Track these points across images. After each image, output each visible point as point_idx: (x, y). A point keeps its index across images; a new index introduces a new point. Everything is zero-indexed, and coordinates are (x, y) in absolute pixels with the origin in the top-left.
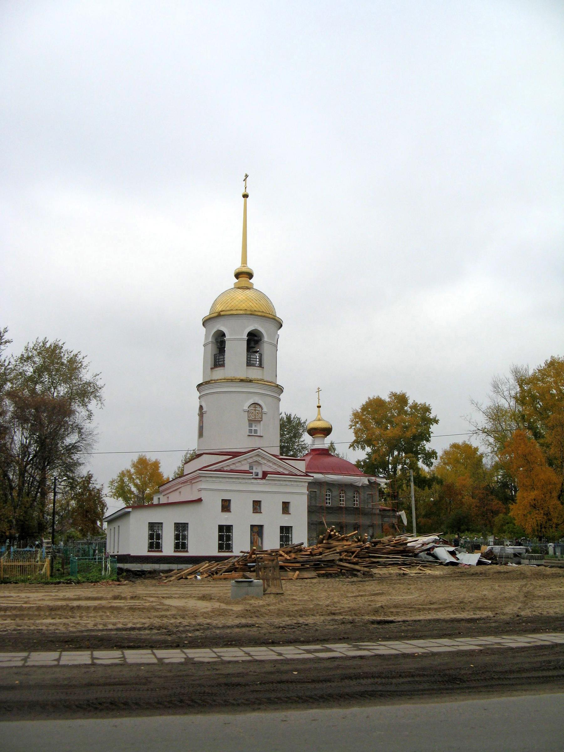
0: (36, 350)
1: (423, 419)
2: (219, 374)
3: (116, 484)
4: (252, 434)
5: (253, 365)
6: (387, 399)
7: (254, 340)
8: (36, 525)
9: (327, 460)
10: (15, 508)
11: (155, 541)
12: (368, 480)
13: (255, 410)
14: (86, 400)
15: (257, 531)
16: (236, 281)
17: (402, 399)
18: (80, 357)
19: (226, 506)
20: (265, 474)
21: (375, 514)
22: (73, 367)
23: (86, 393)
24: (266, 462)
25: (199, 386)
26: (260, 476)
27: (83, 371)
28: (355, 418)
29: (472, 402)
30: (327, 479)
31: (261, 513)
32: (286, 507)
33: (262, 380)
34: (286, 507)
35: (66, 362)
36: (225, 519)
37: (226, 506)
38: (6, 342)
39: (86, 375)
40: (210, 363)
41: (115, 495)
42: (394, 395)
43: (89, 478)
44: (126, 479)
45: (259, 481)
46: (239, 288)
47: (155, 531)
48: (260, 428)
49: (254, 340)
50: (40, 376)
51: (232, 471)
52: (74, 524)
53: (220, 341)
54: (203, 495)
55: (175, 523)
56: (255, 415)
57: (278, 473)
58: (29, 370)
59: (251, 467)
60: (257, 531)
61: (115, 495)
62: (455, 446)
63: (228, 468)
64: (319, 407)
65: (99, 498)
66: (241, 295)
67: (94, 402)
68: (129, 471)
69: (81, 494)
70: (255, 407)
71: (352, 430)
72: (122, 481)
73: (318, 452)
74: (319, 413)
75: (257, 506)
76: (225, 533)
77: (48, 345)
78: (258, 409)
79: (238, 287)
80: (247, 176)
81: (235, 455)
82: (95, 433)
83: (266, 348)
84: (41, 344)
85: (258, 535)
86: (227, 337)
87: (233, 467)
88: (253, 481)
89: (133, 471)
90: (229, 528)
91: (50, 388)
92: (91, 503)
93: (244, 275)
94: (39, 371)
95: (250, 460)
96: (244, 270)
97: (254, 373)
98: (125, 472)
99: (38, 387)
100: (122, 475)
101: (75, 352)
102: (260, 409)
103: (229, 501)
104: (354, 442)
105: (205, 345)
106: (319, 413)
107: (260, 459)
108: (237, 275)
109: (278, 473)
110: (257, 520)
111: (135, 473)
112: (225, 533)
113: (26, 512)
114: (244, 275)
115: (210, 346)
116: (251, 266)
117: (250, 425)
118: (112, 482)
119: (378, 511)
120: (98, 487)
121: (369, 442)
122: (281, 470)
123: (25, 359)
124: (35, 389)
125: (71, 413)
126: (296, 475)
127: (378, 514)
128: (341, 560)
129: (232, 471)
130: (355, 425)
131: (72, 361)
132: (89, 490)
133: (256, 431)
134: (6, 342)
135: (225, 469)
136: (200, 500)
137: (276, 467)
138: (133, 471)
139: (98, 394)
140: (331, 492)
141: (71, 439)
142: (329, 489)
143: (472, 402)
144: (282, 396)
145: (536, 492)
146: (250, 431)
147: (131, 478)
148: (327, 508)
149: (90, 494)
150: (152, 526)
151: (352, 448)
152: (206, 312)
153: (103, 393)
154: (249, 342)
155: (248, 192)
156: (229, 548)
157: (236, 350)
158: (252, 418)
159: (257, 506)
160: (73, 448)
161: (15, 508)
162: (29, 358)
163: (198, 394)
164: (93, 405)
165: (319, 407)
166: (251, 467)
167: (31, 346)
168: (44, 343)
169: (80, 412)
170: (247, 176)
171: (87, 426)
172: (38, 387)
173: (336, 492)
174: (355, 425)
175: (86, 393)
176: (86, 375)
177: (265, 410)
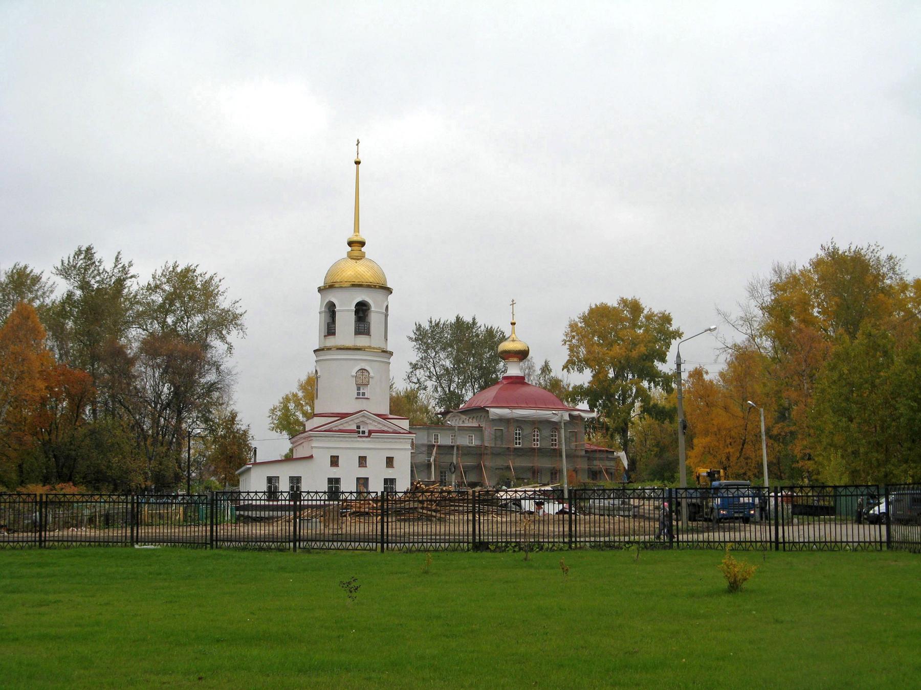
0: (165, 276)
1: (663, 331)
2: (331, 342)
3: (279, 413)
4: (361, 396)
6: (616, 305)
7: (362, 310)
8: (172, 475)
9: (524, 390)
10: (150, 459)
11: (272, 493)
12: (570, 415)
14: (224, 332)
16: (349, 249)
17: (635, 307)
18: (216, 279)
19: (334, 461)
20: (370, 432)
21: (577, 457)
22: (208, 292)
23: (225, 321)
25: (315, 351)
26: (367, 434)
27: (220, 298)
28: (572, 331)
29: (719, 312)
30: (514, 416)
32: (390, 462)
33: (370, 347)
34: (390, 462)
35: (199, 286)
36: (334, 473)
37: (334, 461)
38: (132, 277)
39: (224, 303)
40: (324, 331)
41: (277, 427)
42: (624, 302)
43: (233, 416)
44: (292, 406)
45: (364, 439)
48: (367, 391)
49: (362, 310)
50: (172, 304)
51: (340, 431)
52: (215, 473)
53: (331, 310)
54: (315, 453)
56: (362, 380)
57: (383, 432)
58: (158, 298)
59: (358, 427)
61: (277, 427)
64: (513, 324)
65: (245, 441)
67: (234, 332)
68: (295, 395)
69: (224, 437)
71: (567, 346)
72: (286, 408)
73: (510, 381)
75: (362, 461)
77: (179, 270)
79: (351, 257)
80: (358, 142)
81: (343, 416)
82: (233, 373)
83: (374, 319)
84: (171, 269)
86: (337, 308)
87: (341, 427)
88: (359, 439)
89: (300, 394)
90: (358, 332)
91: (182, 317)
92: (235, 447)
93: (356, 244)
94: (170, 299)
96: (355, 239)
97: (362, 341)
98: (290, 396)
99: (170, 320)
100: (287, 400)
101: (207, 277)
104: (568, 361)
105: (320, 313)
108: (350, 244)
109: (383, 432)
110: (362, 473)
111: (304, 397)
113: (161, 464)
114: (356, 244)
115: (323, 315)
116: (362, 236)
117: (359, 389)
118: (273, 411)
119: (583, 453)
120: (243, 428)
121: (587, 362)
122: (386, 429)
123: (153, 289)
124: (165, 322)
125: (206, 347)
127: (582, 457)
128: (423, 508)
129: (340, 431)
130: (571, 341)
131: (207, 284)
132: (232, 432)
133: (364, 394)
134: (132, 277)
136: (311, 457)
138: (300, 394)
139: (239, 322)
140: (522, 430)
141: (211, 377)
142: (519, 427)
143: (719, 312)
145: (708, 439)
146: (358, 394)
147: (298, 405)
148: (515, 449)
149: (234, 437)
150: (270, 480)
151: (565, 370)
152: (322, 284)
153: (243, 320)
154: (357, 312)
155: (361, 158)
157: (346, 320)
158: (360, 382)
159: (362, 461)
160: (212, 387)
161: (150, 459)
162: (157, 287)
163: (315, 358)
164: (233, 336)
165: (513, 324)
166: (358, 427)
167: (159, 273)
168: (174, 267)
169: (217, 346)
170: (358, 142)
171: (227, 364)
172: (170, 320)
173: (527, 431)
174: (571, 341)
175: (225, 321)
176: (224, 303)
177: (371, 374)
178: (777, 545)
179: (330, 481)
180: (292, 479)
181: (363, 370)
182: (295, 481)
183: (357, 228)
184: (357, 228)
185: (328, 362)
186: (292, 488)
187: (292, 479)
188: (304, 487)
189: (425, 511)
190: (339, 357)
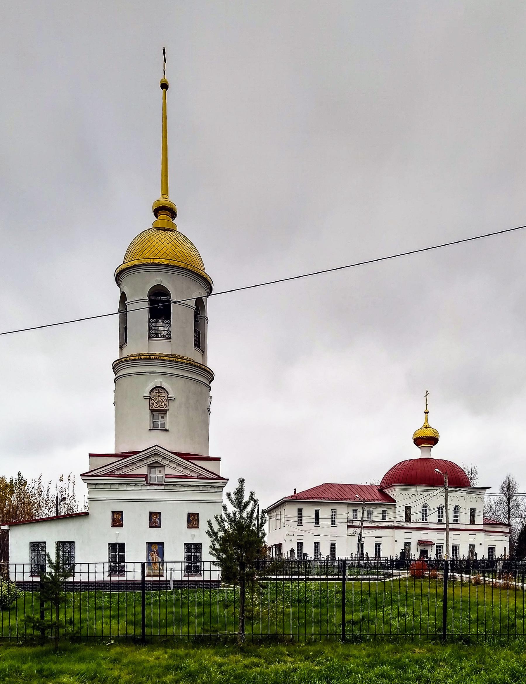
5: (157, 336)
13: (159, 396)
15: (155, 549)
24: (167, 463)
25: (90, 455)
31: (160, 527)
36: (117, 536)
46: (158, 229)
47: (37, 547)
51: (125, 476)
55: (185, 544)
60: (155, 549)
62: (415, 443)
63: (120, 472)
66: (163, 240)
70: (159, 392)
74: (426, 420)
75: (155, 519)
76: (117, 549)
78: (163, 394)
80: (164, 50)
85: (158, 555)
90: (122, 547)
93: (165, 211)
95: (149, 461)
97: (160, 347)
102: (165, 395)
103: (121, 513)
106: (426, 420)
107: (160, 459)
108: (157, 212)
110: (155, 535)
112: (117, 549)
114: (165, 211)
122: (187, 472)
126: (207, 478)
129: (125, 476)
133: (163, 424)
135: (116, 473)
137: (181, 469)
144: (212, 385)
146: (155, 424)
156: (198, 571)
157: (140, 316)
158: (155, 407)
159: (155, 519)
177: (171, 395)
178: (507, 587)
179: (188, 547)
180: (61, 545)
181: (159, 388)
182: (66, 547)
183: (165, 98)
184: (165, 98)
185: (129, 378)
186: (33, 559)
187: (61, 545)
188: (79, 556)
189: (311, 577)
190: (500, 530)
